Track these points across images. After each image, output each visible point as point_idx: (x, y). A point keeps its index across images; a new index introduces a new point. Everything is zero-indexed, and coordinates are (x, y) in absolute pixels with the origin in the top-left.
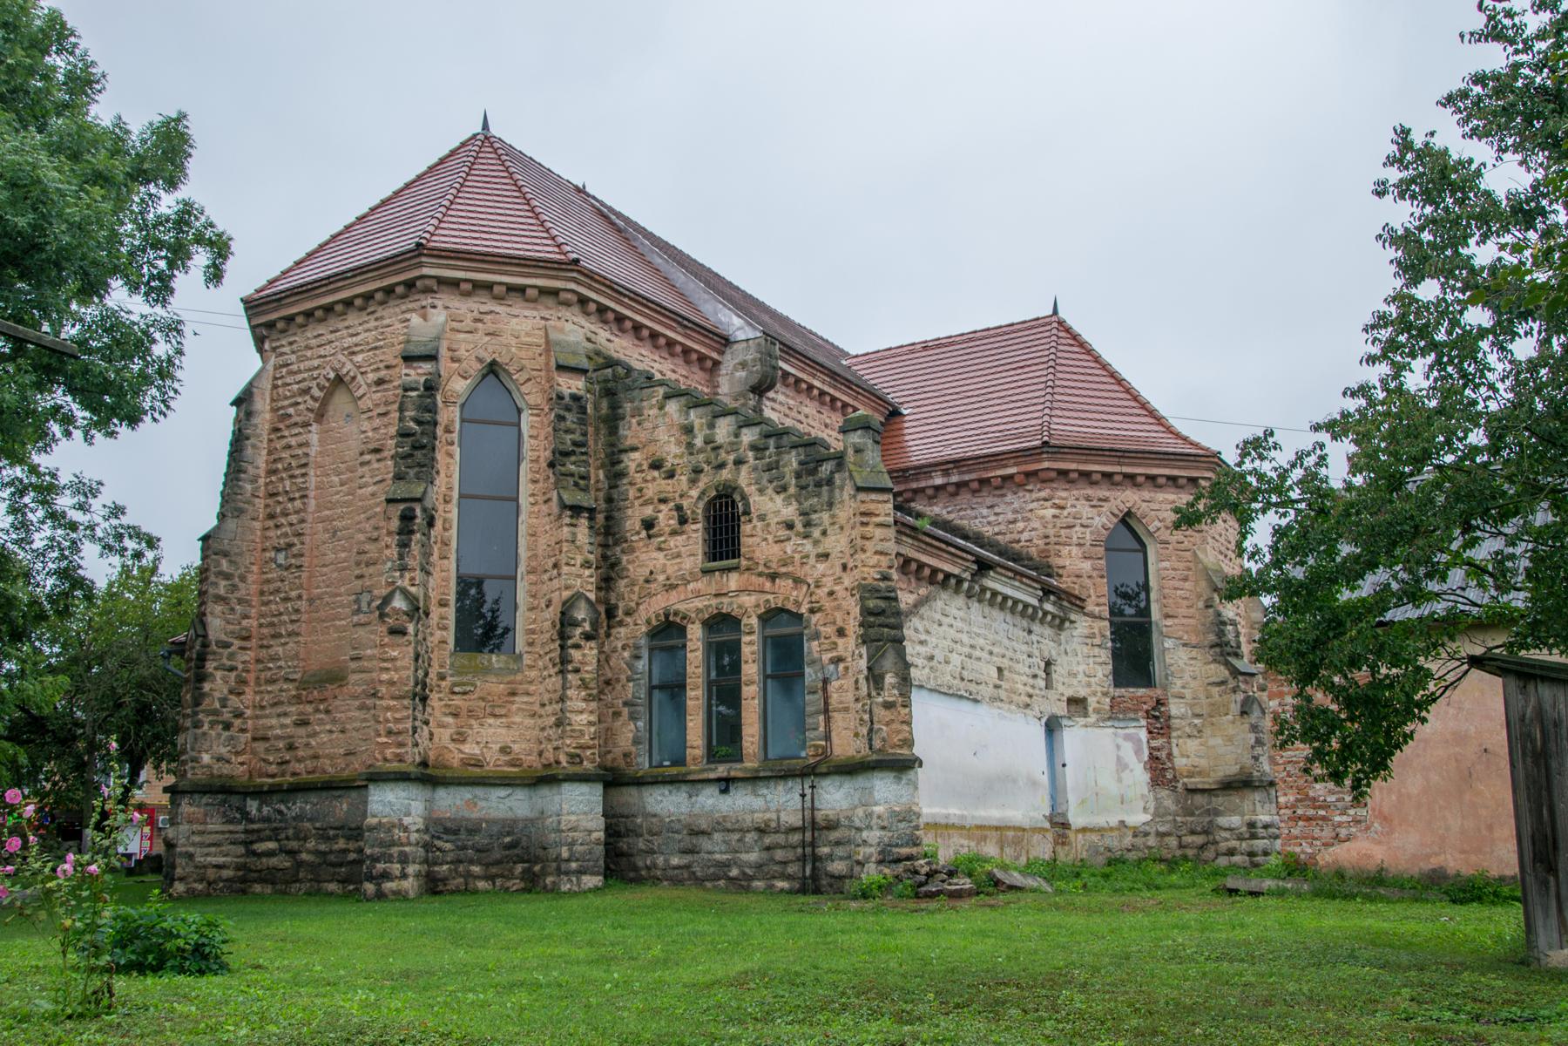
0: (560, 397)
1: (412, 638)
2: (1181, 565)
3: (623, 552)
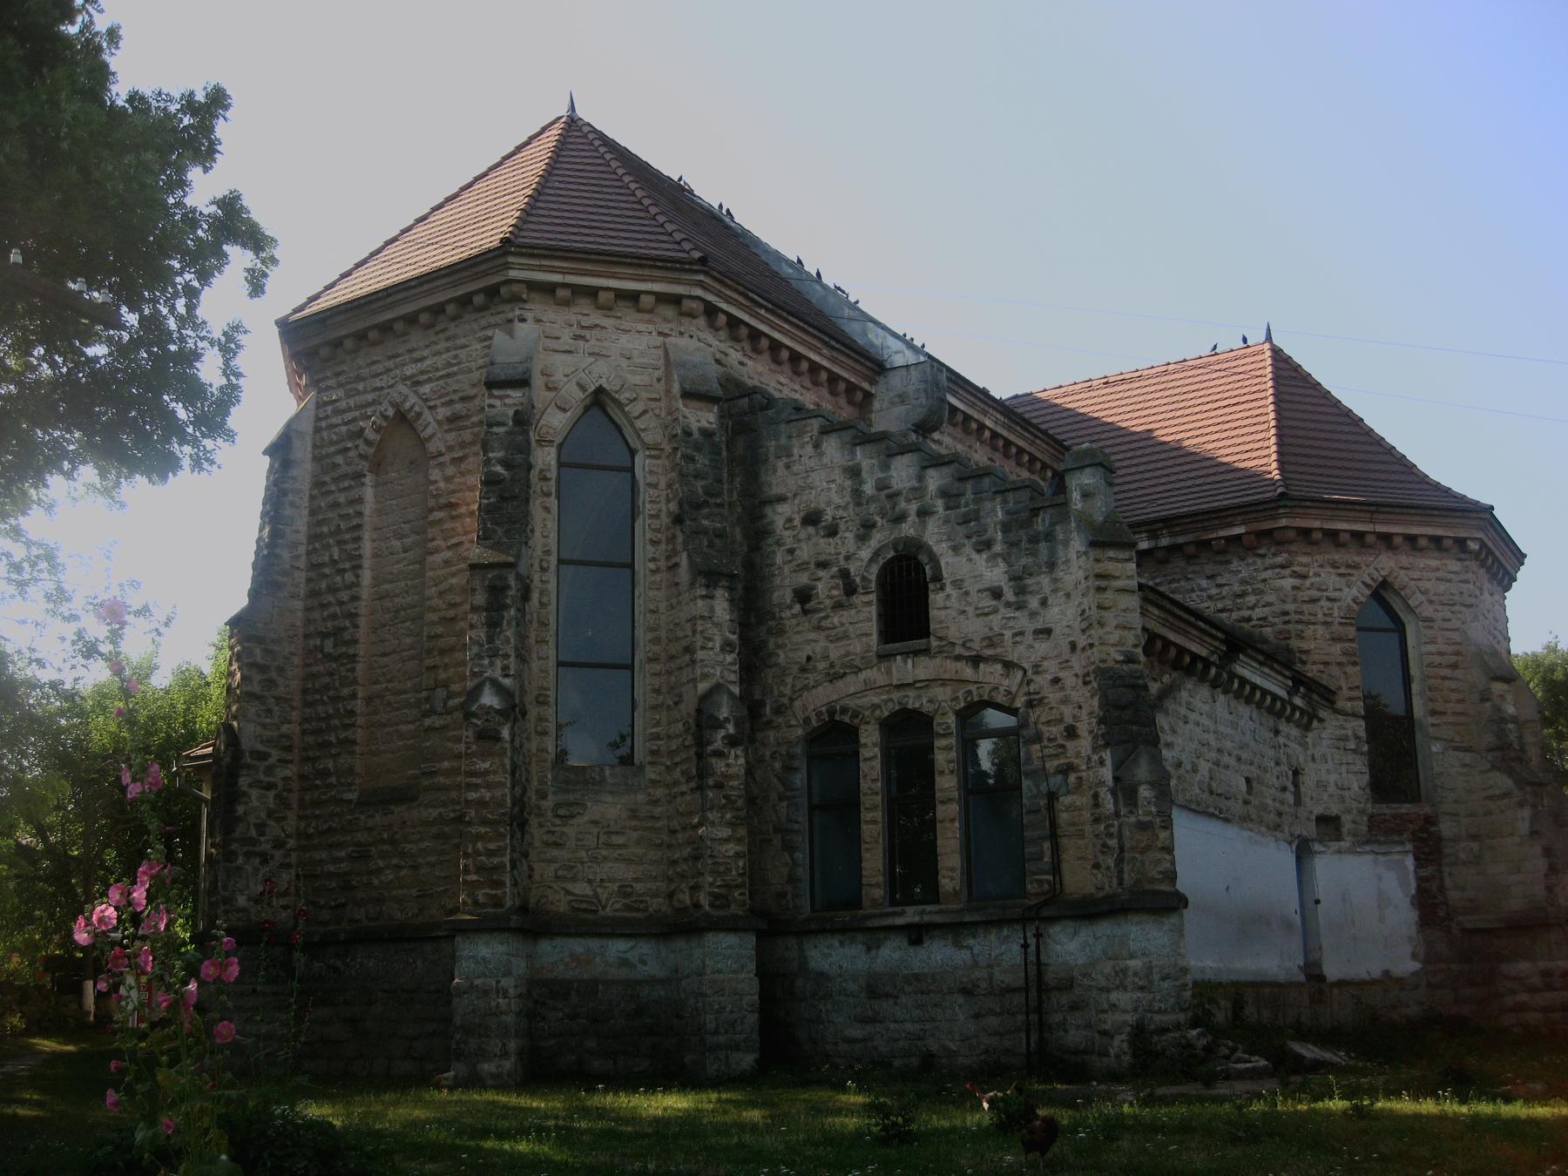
0: (687, 433)
1: (507, 745)
3: (770, 632)
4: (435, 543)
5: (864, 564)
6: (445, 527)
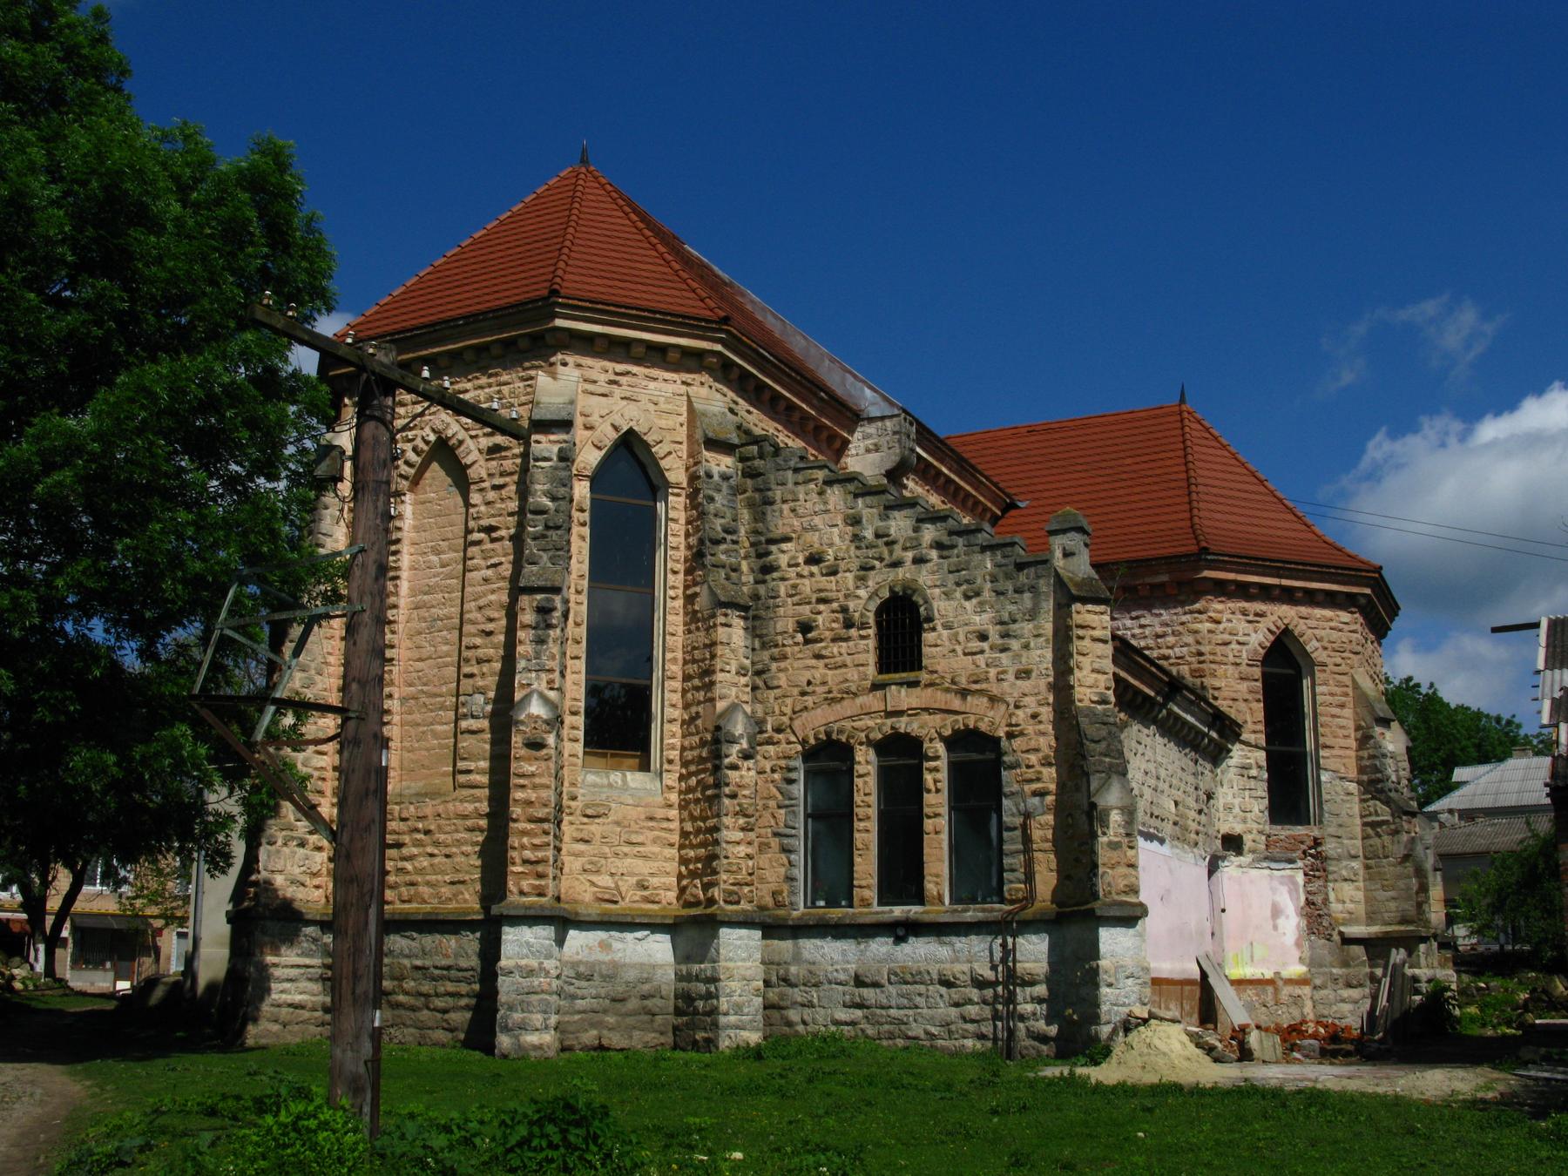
1: (552, 752)
2: (1338, 690)
4: (475, 561)
5: (862, 602)
6: (484, 547)
